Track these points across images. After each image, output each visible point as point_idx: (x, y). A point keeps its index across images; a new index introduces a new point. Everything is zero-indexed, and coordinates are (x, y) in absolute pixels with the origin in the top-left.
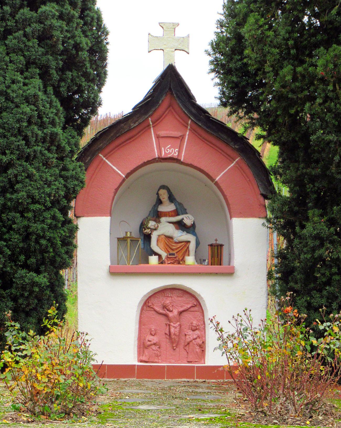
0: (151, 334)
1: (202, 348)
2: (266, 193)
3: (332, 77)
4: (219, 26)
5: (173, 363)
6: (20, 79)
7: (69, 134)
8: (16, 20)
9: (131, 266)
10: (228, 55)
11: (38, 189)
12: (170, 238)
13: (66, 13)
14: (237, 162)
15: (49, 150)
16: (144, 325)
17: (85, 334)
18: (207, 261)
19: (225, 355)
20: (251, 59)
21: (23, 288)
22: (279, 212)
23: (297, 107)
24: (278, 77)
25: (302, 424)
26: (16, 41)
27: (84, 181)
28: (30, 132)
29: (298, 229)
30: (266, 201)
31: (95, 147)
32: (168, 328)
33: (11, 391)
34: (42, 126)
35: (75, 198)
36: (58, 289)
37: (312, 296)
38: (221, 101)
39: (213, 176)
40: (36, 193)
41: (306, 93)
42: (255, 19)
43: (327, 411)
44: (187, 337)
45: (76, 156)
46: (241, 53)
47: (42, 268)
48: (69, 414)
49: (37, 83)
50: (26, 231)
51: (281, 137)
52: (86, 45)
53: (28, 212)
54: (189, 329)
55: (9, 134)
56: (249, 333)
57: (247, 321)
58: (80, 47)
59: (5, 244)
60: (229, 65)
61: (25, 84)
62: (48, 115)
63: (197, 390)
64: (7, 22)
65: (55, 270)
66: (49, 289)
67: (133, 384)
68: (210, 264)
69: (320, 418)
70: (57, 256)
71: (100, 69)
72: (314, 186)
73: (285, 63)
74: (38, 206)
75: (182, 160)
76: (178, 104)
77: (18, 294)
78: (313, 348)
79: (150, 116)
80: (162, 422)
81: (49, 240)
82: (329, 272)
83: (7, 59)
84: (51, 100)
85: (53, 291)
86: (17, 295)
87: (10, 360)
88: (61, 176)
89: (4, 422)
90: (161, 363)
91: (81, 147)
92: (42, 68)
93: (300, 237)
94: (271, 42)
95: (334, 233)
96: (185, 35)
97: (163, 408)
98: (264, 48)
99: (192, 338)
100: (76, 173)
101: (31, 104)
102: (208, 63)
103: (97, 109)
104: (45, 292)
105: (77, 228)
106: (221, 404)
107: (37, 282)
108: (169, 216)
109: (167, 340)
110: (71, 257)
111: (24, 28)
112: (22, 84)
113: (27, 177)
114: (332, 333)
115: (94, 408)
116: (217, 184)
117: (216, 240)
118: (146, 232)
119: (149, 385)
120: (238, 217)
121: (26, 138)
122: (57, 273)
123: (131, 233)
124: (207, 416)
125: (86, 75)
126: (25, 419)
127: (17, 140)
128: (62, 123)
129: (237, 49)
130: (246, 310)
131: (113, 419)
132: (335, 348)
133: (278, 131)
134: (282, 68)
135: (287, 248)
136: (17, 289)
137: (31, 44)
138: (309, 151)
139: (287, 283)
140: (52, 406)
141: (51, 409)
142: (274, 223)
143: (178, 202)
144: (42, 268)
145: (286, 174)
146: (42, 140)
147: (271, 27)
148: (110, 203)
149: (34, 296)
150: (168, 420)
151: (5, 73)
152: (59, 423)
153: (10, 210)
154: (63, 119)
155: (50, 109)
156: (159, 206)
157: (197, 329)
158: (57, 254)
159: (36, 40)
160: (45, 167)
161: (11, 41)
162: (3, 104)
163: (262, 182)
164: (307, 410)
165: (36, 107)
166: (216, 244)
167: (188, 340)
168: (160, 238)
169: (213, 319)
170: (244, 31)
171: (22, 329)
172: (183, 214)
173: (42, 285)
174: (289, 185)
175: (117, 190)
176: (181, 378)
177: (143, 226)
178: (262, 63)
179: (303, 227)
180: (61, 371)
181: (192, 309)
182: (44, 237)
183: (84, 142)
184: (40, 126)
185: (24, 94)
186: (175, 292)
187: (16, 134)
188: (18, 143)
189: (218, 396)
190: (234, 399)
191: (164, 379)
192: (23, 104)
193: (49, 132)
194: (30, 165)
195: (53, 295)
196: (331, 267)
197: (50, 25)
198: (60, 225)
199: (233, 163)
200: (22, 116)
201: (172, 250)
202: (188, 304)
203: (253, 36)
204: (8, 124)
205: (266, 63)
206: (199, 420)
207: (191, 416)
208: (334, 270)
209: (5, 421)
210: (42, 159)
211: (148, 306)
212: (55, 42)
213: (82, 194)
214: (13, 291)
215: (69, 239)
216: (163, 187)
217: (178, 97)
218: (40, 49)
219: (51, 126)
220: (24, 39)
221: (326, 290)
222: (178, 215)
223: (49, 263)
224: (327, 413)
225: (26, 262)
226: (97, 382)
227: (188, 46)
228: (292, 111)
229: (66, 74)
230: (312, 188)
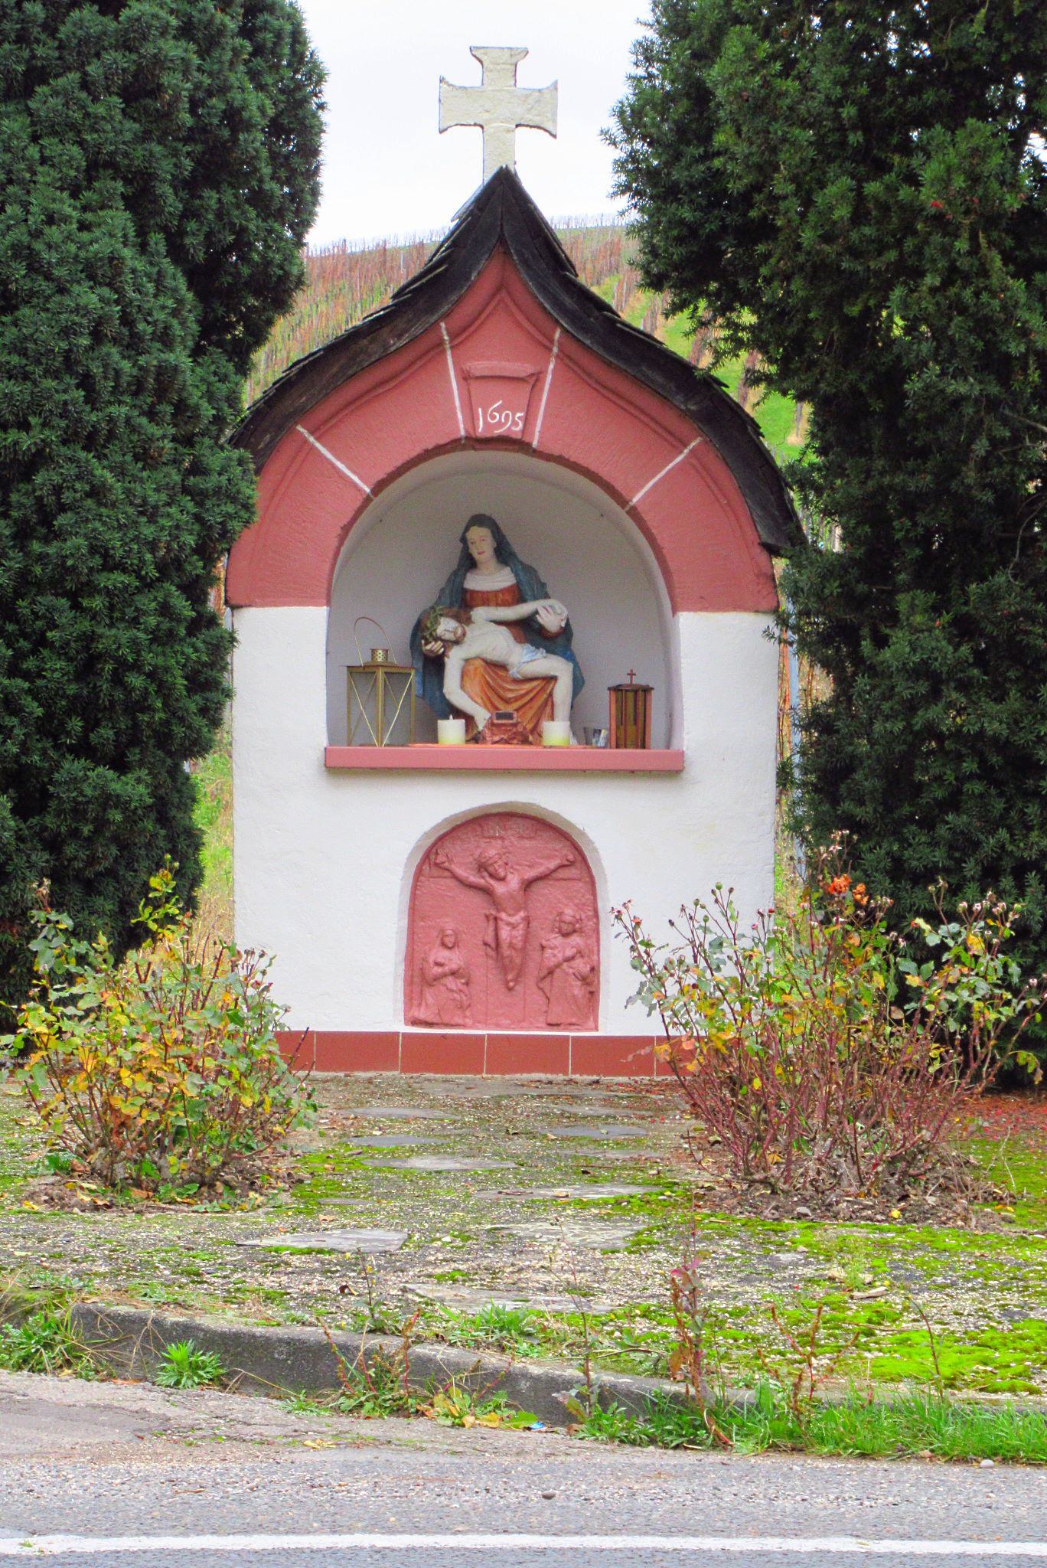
0: (444, 945)
1: (588, 984)
2: (777, 539)
3: (967, 212)
4: (641, 58)
5: (507, 1028)
6: (68, 210)
7: (213, 368)
8: (60, 41)
9: (382, 751)
10: (669, 146)
11: (121, 527)
12: (498, 667)
13: (200, 21)
14: (691, 451)
15: (152, 415)
16: (423, 919)
17: (257, 953)
18: (604, 733)
19: (656, 1012)
20: (733, 158)
21: (78, 811)
22: (812, 599)
23: (865, 296)
24: (812, 209)
25: (879, 1217)
26: (60, 100)
27: (253, 506)
28: (98, 363)
29: (866, 646)
30: (775, 561)
31: (287, 405)
32: (491, 929)
33: (46, 1118)
34: (133, 345)
35: (229, 551)
36: (179, 815)
37: (907, 840)
38: (647, 272)
39: (624, 493)
40: (114, 540)
41: (892, 255)
42: (744, 43)
43: (950, 1179)
44: (548, 953)
45: (228, 432)
46: (706, 138)
47: (134, 755)
48: (212, 1186)
49: (117, 222)
50: (87, 648)
51: (817, 382)
52: (258, 114)
53: (91, 595)
54: (552, 931)
55: (39, 371)
56: (730, 958)
57: (722, 920)
58: (241, 120)
59: (26, 685)
60: (669, 174)
61: (83, 226)
62: (150, 314)
63: (575, 1109)
64: (35, 46)
65: (169, 761)
66: (153, 815)
67: (391, 1091)
68: (614, 743)
69: (931, 1200)
70: (174, 721)
71: (300, 179)
72: (915, 524)
73: (832, 170)
74: (119, 578)
75: (535, 444)
76: (525, 285)
77: (63, 829)
78: (905, 993)
79: (446, 316)
80: (479, 1211)
81: (151, 676)
82: (954, 771)
83: (33, 152)
84: (159, 272)
85: (163, 820)
86: (59, 834)
87: (43, 1029)
88: (186, 490)
89: (25, 1208)
90: (471, 1028)
91: (246, 406)
92: (134, 178)
93: (873, 671)
94: (791, 109)
95: (971, 660)
96: (544, 83)
97: (480, 1165)
98: (771, 129)
99: (560, 956)
100: (229, 480)
101: (101, 284)
102: (610, 167)
103: (290, 296)
104: (140, 825)
105: (233, 639)
106: (645, 1154)
107: (118, 796)
108: (497, 605)
109: (490, 962)
110: (216, 723)
111: (83, 65)
112: (75, 226)
113: (88, 495)
114: (963, 955)
115: (283, 1166)
116: (634, 513)
117: (631, 674)
118: (431, 651)
119: (438, 1091)
120: (695, 610)
121: (86, 382)
122: (175, 771)
123: (386, 651)
124: (605, 1192)
125: (259, 200)
126: (87, 1199)
127: (62, 387)
128: (189, 338)
129: (694, 126)
130: (719, 888)
131: (338, 1201)
132: (972, 1000)
133: (811, 365)
134: (822, 185)
135: (835, 701)
136: (59, 815)
137: (101, 110)
138: (901, 422)
139: (835, 801)
140: (161, 1162)
141: (159, 1170)
142: (797, 629)
143: (521, 563)
144: (134, 755)
145: (832, 488)
146: (133, 388)
147: (789, 65)
148: (327, 567)
149: (108, 834)
150: (496, 1204)
151: (28, 192)
152: (182, 1211)
153: (40, 587)
154: (195, 327)
155: (155, 296)
156: (468, 575)
157: (575, 931)
158: (175, 715)
159: (116, 100)
160: (140, 465)
161: (45, 101)
162: (21, 282)
163: (763, 508)
164: (892, 1175)
165: (116, 292)
166: (631, 685)
167: (553, 961)
168: (471, 668)
169: (623, 910)
170: (713, 74)
171: (73, 934)
172: (535, 598)
173: (133, 806)
174: (844, 519)
175: (346, 529)
176: (529, 1071)
177: (421, 631)
178: (766, 169)
179: (881, 642)
180: (188, 1061)
181: (562, 874)
182: (136, 667)
183: (251, 392)
184: (128, 347)
185: (82, 254)
186: (511, 823)
187: (57, 371)
188: (66, 397)
189: (634, 1129)
190: (682, 1137)
191: (480, 1072)
192: (79, 283)
193: (155, 363)
194: (99, 459)
195: (163, 832)
196: (960, 758)
197: (155, 56)
198: (182, 632)
199: (681, 452)
200: (77, 319)
201: (507, 701)
202: (550, 857)
203: (738, 94)
204: (35, 342)
205: (776, 169)
206: (583, 1205)
207: (560, 1191)
208: (969, 766)
209: (28, 1205)
210: (131, 442)
211: (436, 864)
212: (169, 105)
213: (246, 541)
214: (50, 821)
215: (210, 673)
216: (479, 520)
217: (525, 262)
218: (129, 124)
219: (158, 345)
220: (84, 95)
221: (947, 823)
222: (520, 599)
223: (152, 741)
224: (950, 1184)
225: (87, 737)
226: (293, 1087)
227: (555, 114)
228: (854, 310)
229: (201, 197)
230: (908, 531)
